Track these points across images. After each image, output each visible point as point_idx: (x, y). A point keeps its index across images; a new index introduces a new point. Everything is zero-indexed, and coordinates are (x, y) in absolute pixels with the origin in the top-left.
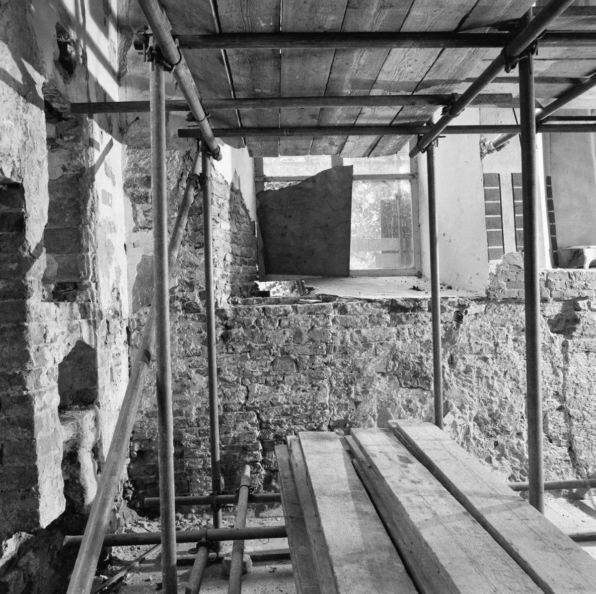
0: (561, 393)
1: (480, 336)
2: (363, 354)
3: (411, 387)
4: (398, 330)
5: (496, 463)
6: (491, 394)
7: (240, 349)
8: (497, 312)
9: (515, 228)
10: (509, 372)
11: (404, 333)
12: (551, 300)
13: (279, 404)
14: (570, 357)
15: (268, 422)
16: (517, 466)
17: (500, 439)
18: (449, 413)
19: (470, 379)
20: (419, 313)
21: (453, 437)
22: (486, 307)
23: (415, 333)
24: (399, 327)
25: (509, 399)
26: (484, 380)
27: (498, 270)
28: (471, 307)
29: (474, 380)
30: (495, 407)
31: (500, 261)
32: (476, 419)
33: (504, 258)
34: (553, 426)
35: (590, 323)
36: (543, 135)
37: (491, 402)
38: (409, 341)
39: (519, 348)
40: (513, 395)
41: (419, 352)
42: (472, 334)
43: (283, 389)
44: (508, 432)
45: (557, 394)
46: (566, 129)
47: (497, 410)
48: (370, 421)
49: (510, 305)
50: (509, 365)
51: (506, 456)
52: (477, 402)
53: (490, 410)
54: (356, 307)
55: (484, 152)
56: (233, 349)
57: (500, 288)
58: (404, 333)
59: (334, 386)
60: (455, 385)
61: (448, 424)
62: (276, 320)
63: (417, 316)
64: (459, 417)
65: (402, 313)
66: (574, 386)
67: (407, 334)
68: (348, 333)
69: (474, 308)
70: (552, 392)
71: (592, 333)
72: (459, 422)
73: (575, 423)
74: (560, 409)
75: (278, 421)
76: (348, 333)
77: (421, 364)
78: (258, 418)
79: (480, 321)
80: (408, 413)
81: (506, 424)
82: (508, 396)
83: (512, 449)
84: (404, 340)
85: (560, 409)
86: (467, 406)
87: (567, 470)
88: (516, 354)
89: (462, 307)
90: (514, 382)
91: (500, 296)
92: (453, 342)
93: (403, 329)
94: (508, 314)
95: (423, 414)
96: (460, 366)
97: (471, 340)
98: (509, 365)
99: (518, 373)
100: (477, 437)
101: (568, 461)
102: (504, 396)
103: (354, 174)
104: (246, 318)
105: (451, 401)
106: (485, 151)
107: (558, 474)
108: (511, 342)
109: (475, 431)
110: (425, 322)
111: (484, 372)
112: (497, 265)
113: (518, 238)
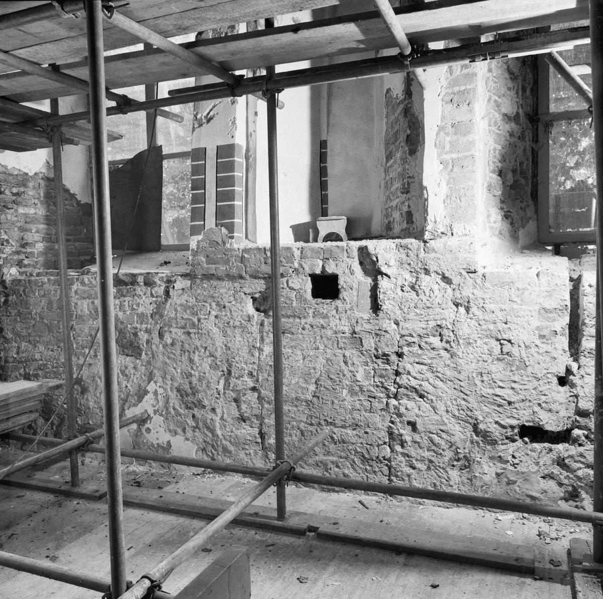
0: (255, 374)
1: (185, 311)
2: (95, 323)
3: (127, 355)
4: (120, 302)
5: (189, 434)
6: (192, 368)
7: (14, 312)
8: (200, 287)
9: (217, 202)
10: (208, 348)
11: (124, 305)
12: (248, 277)
13: (36, 360)
14: (265, 338)
15: (29, 374)
16: (208, 440)
17: (196, 411)
18: (152, 382)
19: (174, 352)
20: (136, 287)
21: (155, 404)
22: (192, 282)
23: (132, 306)
24: (122, 299)
25: (207, 374)
26: (187, 354)
27: (198, 246)
28: (177, 282)
29: (178, 352)
30: (194, 380)
31: (200, 237)
32: (178, 390)
33: (204, 234)
34: (246, 406)
35: (288, 302)
36: (147, 114)
37: (191, 375)
38: (128, 313)
39: (219, 324)
40: (212, 371)
41: (135, 323)
42: (179, 309)
43: (38, 348)
44: (204, 407)
45: (251, 374)
46: (171, 102)
47: (196, 384)
48: (97, 382)
49: (212, 282)
50: (209, 341)
51: (199, 429)
52: (179, 374)
53: (190, 383)
54: (91, 280)
55: (195, 126)
56: (10, 313)
57: (199, 265)
58: (124, 305)
59: (75, 348)
60: (160, 356)
61: (151, 392)
62: (35, 290)
63: (134, 290)
64: (160, 387)
65: (124, 287)
66: (549, 380)
67: (127, 306)
68: (85, 303)
69: (180, 284)
70: (246, 372)
71: (289, 314)
72: (160, 391)
73: (266, 406)
74: (254, 389)
75: (36, 374)
76: (85, 303)
77: (136, 334)
78: (24, 370)
79: (185, 297)
80: (125, 377)
81: (203, 398)
82: (207, 372)
83: (205, 423)
84: (125, 311)
85: (254, 389)
86: (169, 377)
87: (256, 453)
88: (215, 330)
89: (169, 282)
90: (212, 358)
91: (199, 272)
92: (161, 316)
93: (124, 301)
94: (210, 290)
95: (135, 381)
96: (167, 339)
97: (178, 315)
98: (209, 341)
99: (216, 350)
100: (177, 407)
101: (258, 443)
102: (203, 371)
103: (163, 153)
104: (17, 287)
105: (155, 371)
106: (196, 126)
107: (246, 454)
108: (212, 318)
109: (175, 401)
110: (140, 295)
111: (187, 346)
112: (198, 242)
113: (218, 213)
